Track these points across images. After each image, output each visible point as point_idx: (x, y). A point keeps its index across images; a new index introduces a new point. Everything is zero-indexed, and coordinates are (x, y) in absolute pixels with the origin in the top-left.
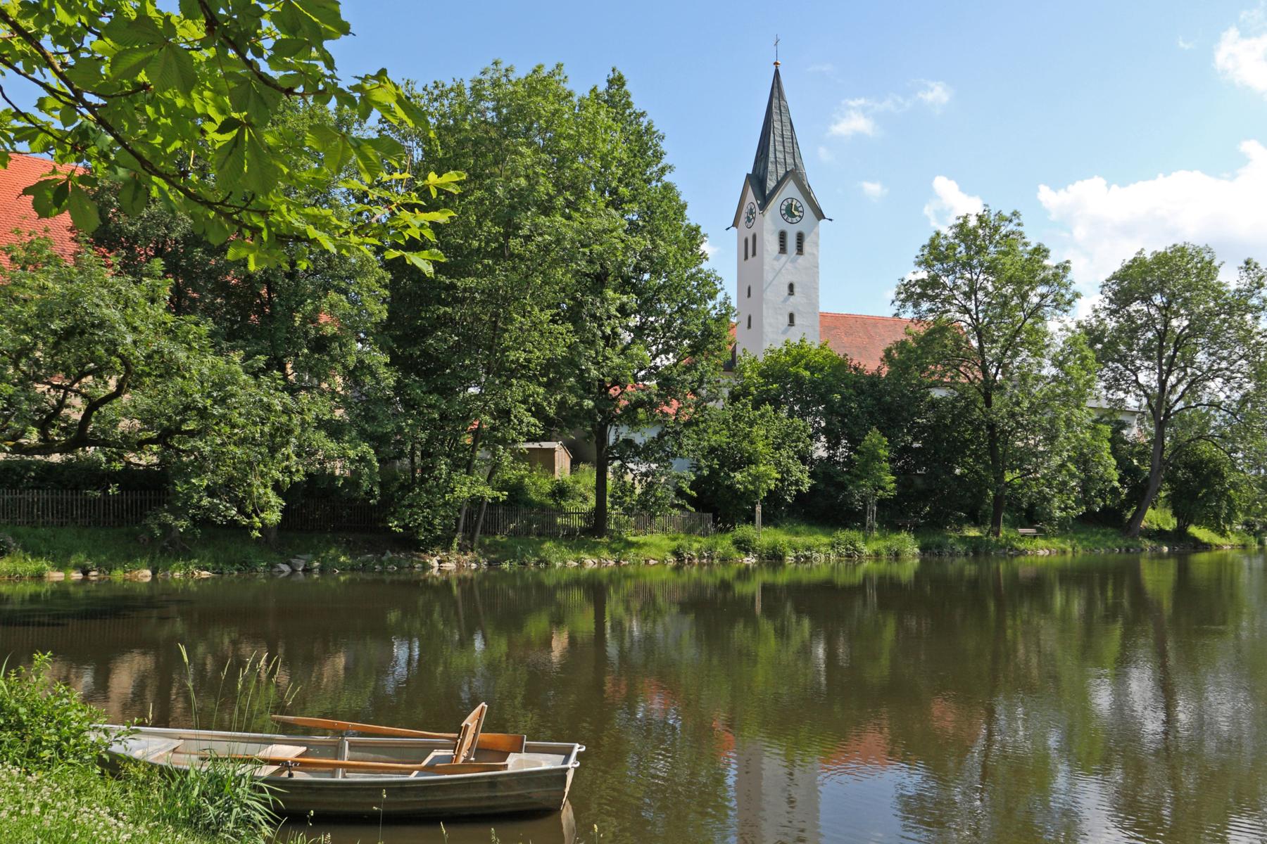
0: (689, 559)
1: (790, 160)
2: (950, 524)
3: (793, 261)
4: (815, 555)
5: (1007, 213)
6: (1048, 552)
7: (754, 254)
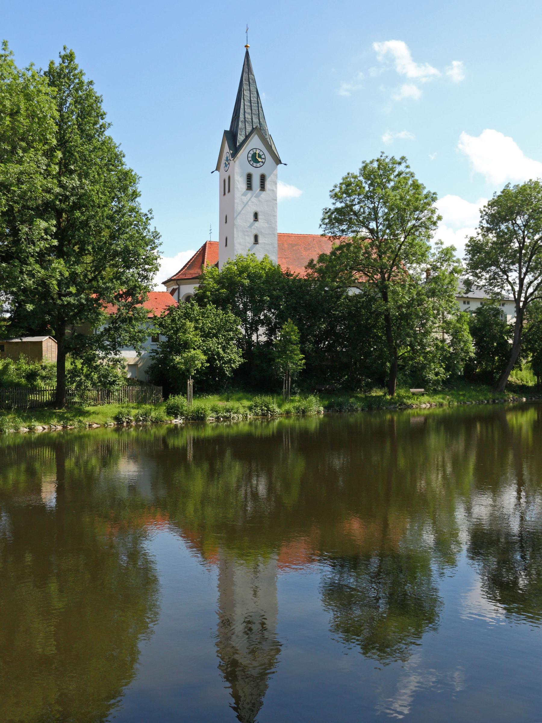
0: (127, 422)
1: (255, 120)
2: (360, 387)
3: (257, 196)
4: (232, 415)
5: (398, 159)
6: (429, 405)
7: (229, 191)
